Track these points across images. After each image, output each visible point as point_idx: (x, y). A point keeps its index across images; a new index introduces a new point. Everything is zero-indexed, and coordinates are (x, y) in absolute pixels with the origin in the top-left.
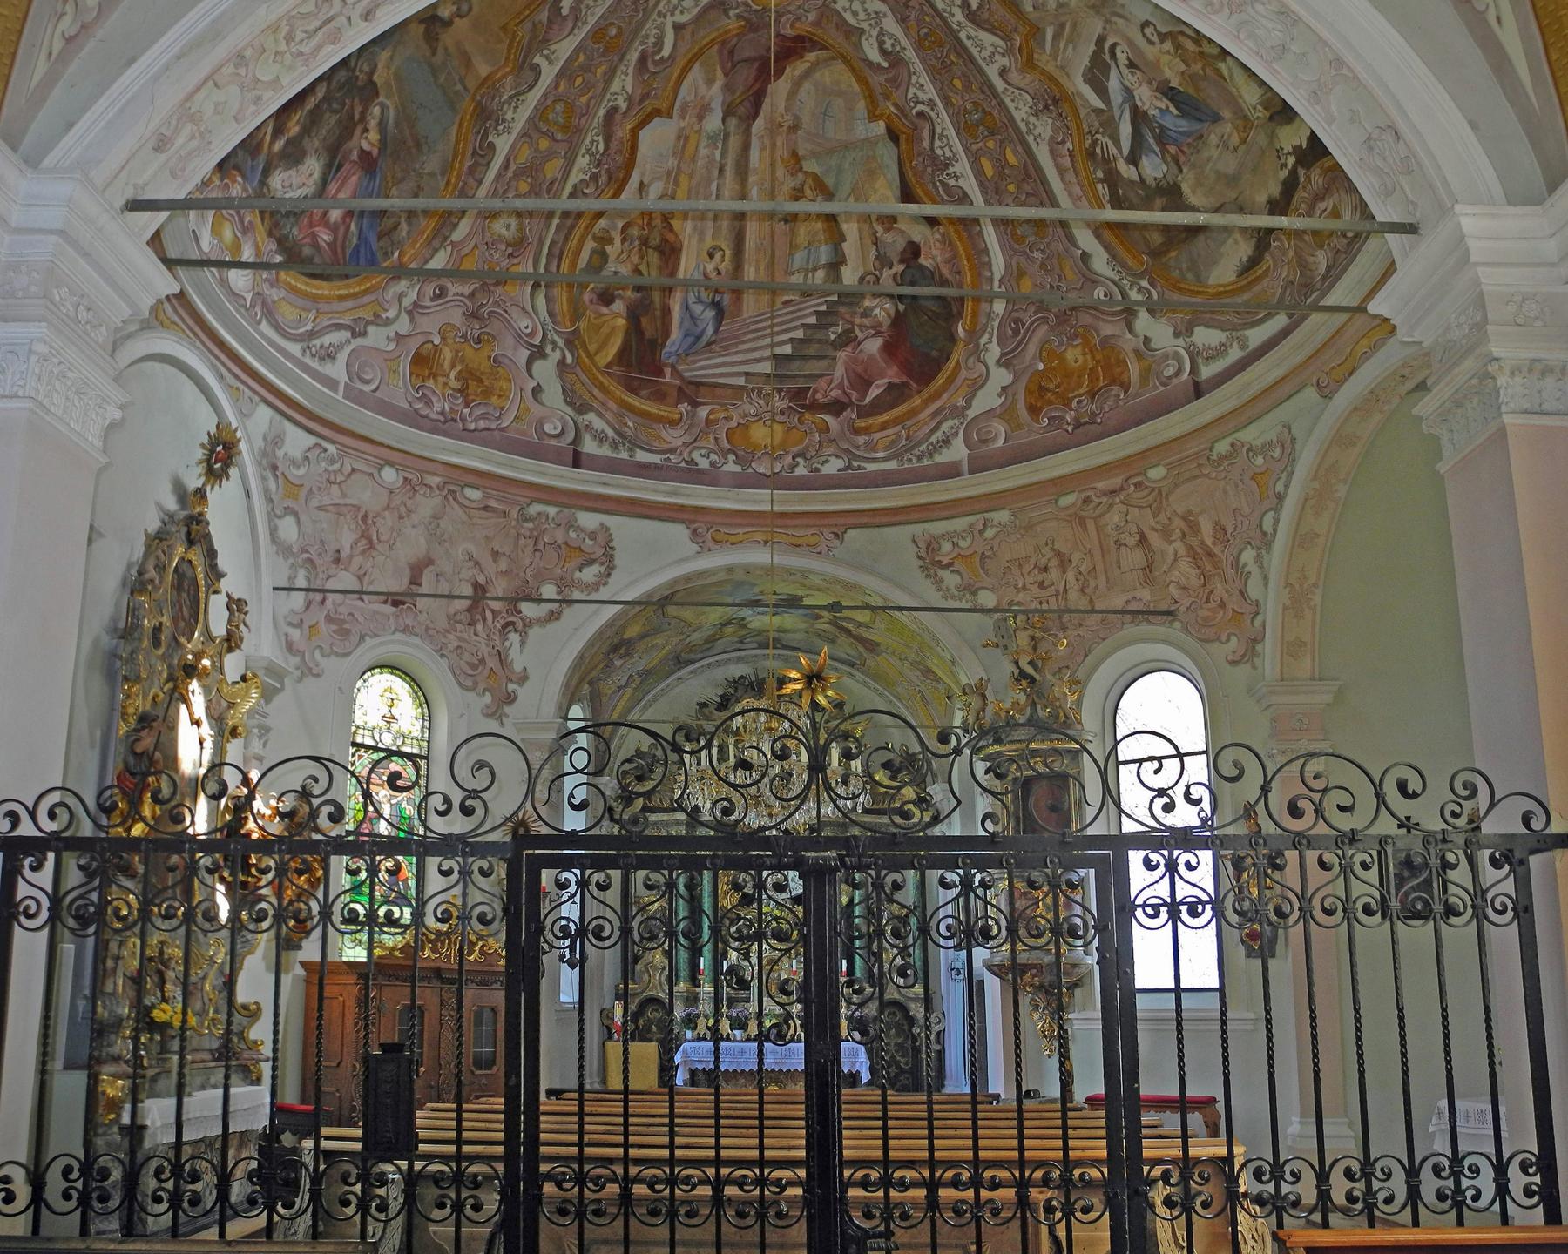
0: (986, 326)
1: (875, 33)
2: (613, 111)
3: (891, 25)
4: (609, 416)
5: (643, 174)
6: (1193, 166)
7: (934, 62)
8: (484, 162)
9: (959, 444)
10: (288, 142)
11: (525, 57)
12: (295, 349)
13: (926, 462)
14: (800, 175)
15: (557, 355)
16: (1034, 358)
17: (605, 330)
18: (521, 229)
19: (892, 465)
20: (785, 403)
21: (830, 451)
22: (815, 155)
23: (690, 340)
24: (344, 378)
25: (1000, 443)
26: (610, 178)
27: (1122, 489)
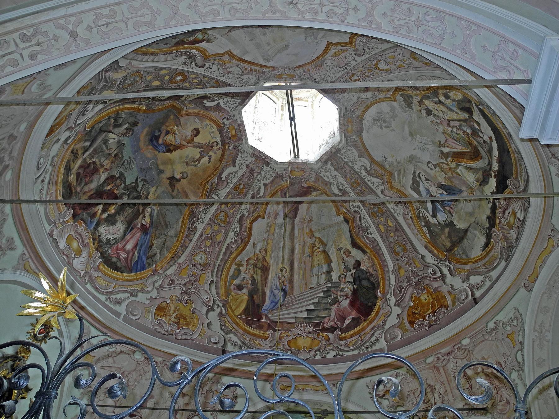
0: (388, 291)
1: (335, 183)
2: (243, 216)
3: (341, 179)
4: (239, 335)
5: (254, 240)
6: (456, 213)
7: (358, 191)
8: (193, 233)
9: (382, 340)
10: (109, 215)
11: (209, 195)
12: (103, 298)
13: (370, 350)
14: (314, 239)
15: (219, 310)
16: (409, 301)
17: (239, 300)
18: (207, 259)
19: (356, 352)
20: (312, 329)
21: (330, 348)
22: (319, 230)
23: (273, 304)
24: (124, 312)
25: (399, 338)
26: (242, 241)
27: (452, 351)
